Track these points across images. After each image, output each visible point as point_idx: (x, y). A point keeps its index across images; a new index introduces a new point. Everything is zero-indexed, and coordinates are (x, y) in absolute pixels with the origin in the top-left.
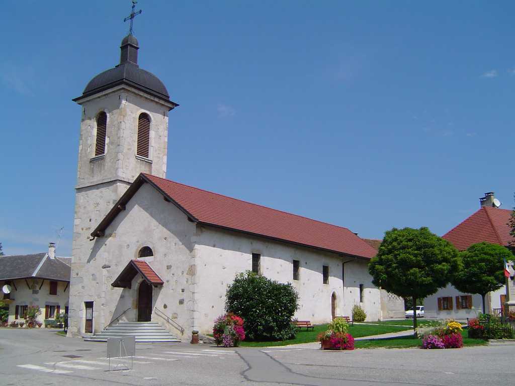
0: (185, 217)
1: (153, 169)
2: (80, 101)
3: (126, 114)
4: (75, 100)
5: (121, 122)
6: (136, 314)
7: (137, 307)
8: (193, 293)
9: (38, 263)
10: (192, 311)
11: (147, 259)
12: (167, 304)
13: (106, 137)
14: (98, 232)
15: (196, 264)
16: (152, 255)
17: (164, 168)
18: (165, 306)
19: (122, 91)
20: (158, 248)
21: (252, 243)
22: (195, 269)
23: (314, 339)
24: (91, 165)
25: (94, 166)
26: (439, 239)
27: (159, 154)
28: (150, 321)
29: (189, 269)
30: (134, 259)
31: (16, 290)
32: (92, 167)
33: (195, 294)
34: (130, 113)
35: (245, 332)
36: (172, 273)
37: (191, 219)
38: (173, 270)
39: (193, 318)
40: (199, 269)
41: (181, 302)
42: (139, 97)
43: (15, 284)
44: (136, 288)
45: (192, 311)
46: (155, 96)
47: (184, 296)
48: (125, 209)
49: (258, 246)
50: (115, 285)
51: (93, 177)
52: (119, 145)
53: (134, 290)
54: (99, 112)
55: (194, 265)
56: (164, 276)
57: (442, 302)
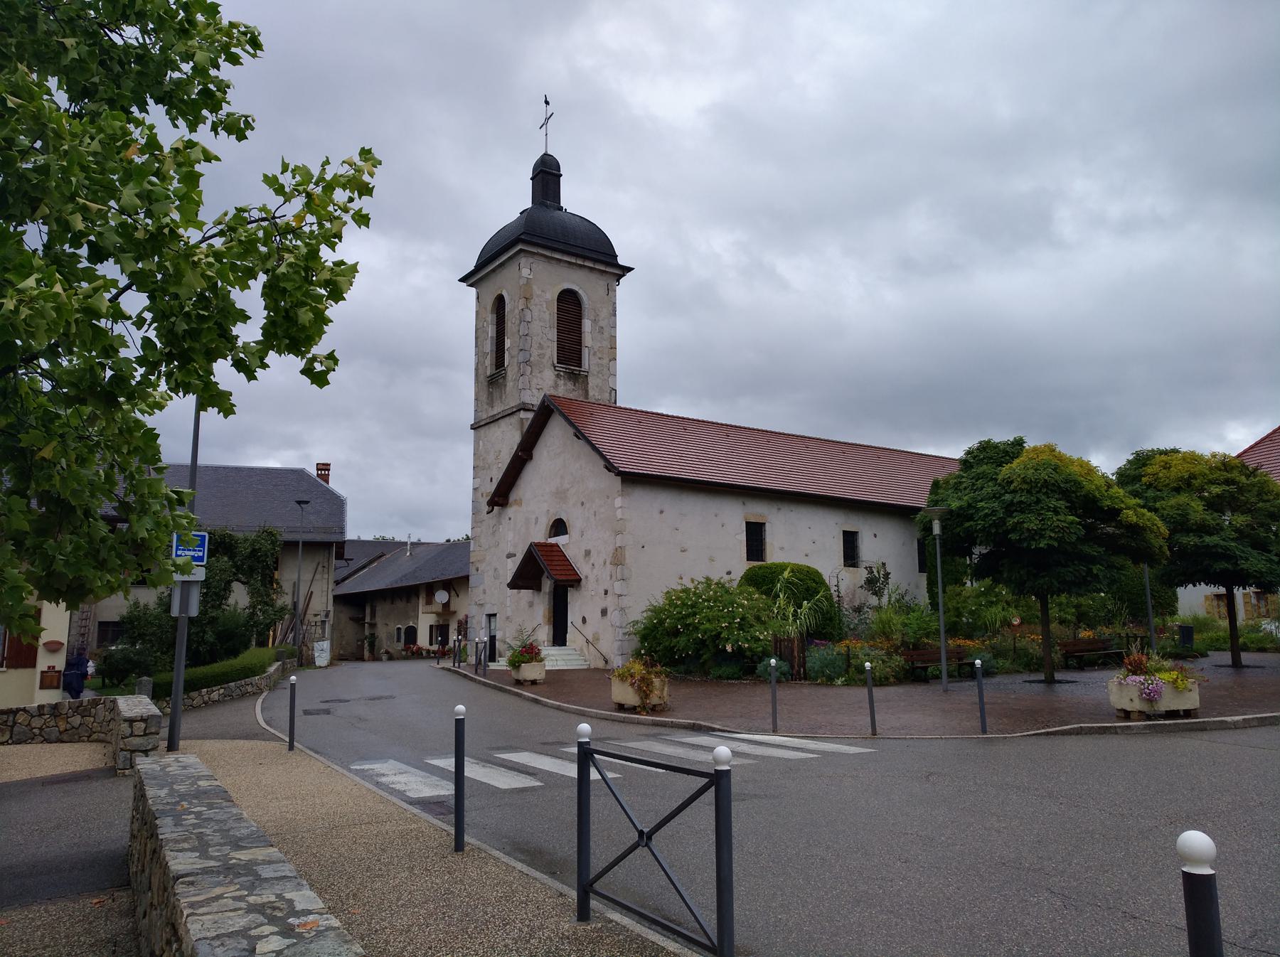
0: (602, 463)
1: (590, 384)
2: (471, 281)
3: (532, 295)
4: (462, 280)
6: (548, 634)
7: (548, 621)
11: (561, 540)
14: (496, 499)
16: (566, 533)
18: (584, 620)
19: (522, 255)
20: (575, 521)
21: (744, 504)
23: (1221, 714)
24: (489, 388)
25: (492, 388)
27: (600, 358)
28: (565, 645)
29: (614, 554)
31: (458, 596)
32: (491, 390)
34: (539, 292)
36: (592, 561)
37: (610, 467)
41: (604, 612)
42: (554, 262)
43: (456, 589)
44: (548, 591)
46: (585, 258)
47: (610, 602)
48: (531, 458)
49: (758, 511)
50: (514, 585)
51: (492, 407)
53: (545, 593)
56: (583, 568)
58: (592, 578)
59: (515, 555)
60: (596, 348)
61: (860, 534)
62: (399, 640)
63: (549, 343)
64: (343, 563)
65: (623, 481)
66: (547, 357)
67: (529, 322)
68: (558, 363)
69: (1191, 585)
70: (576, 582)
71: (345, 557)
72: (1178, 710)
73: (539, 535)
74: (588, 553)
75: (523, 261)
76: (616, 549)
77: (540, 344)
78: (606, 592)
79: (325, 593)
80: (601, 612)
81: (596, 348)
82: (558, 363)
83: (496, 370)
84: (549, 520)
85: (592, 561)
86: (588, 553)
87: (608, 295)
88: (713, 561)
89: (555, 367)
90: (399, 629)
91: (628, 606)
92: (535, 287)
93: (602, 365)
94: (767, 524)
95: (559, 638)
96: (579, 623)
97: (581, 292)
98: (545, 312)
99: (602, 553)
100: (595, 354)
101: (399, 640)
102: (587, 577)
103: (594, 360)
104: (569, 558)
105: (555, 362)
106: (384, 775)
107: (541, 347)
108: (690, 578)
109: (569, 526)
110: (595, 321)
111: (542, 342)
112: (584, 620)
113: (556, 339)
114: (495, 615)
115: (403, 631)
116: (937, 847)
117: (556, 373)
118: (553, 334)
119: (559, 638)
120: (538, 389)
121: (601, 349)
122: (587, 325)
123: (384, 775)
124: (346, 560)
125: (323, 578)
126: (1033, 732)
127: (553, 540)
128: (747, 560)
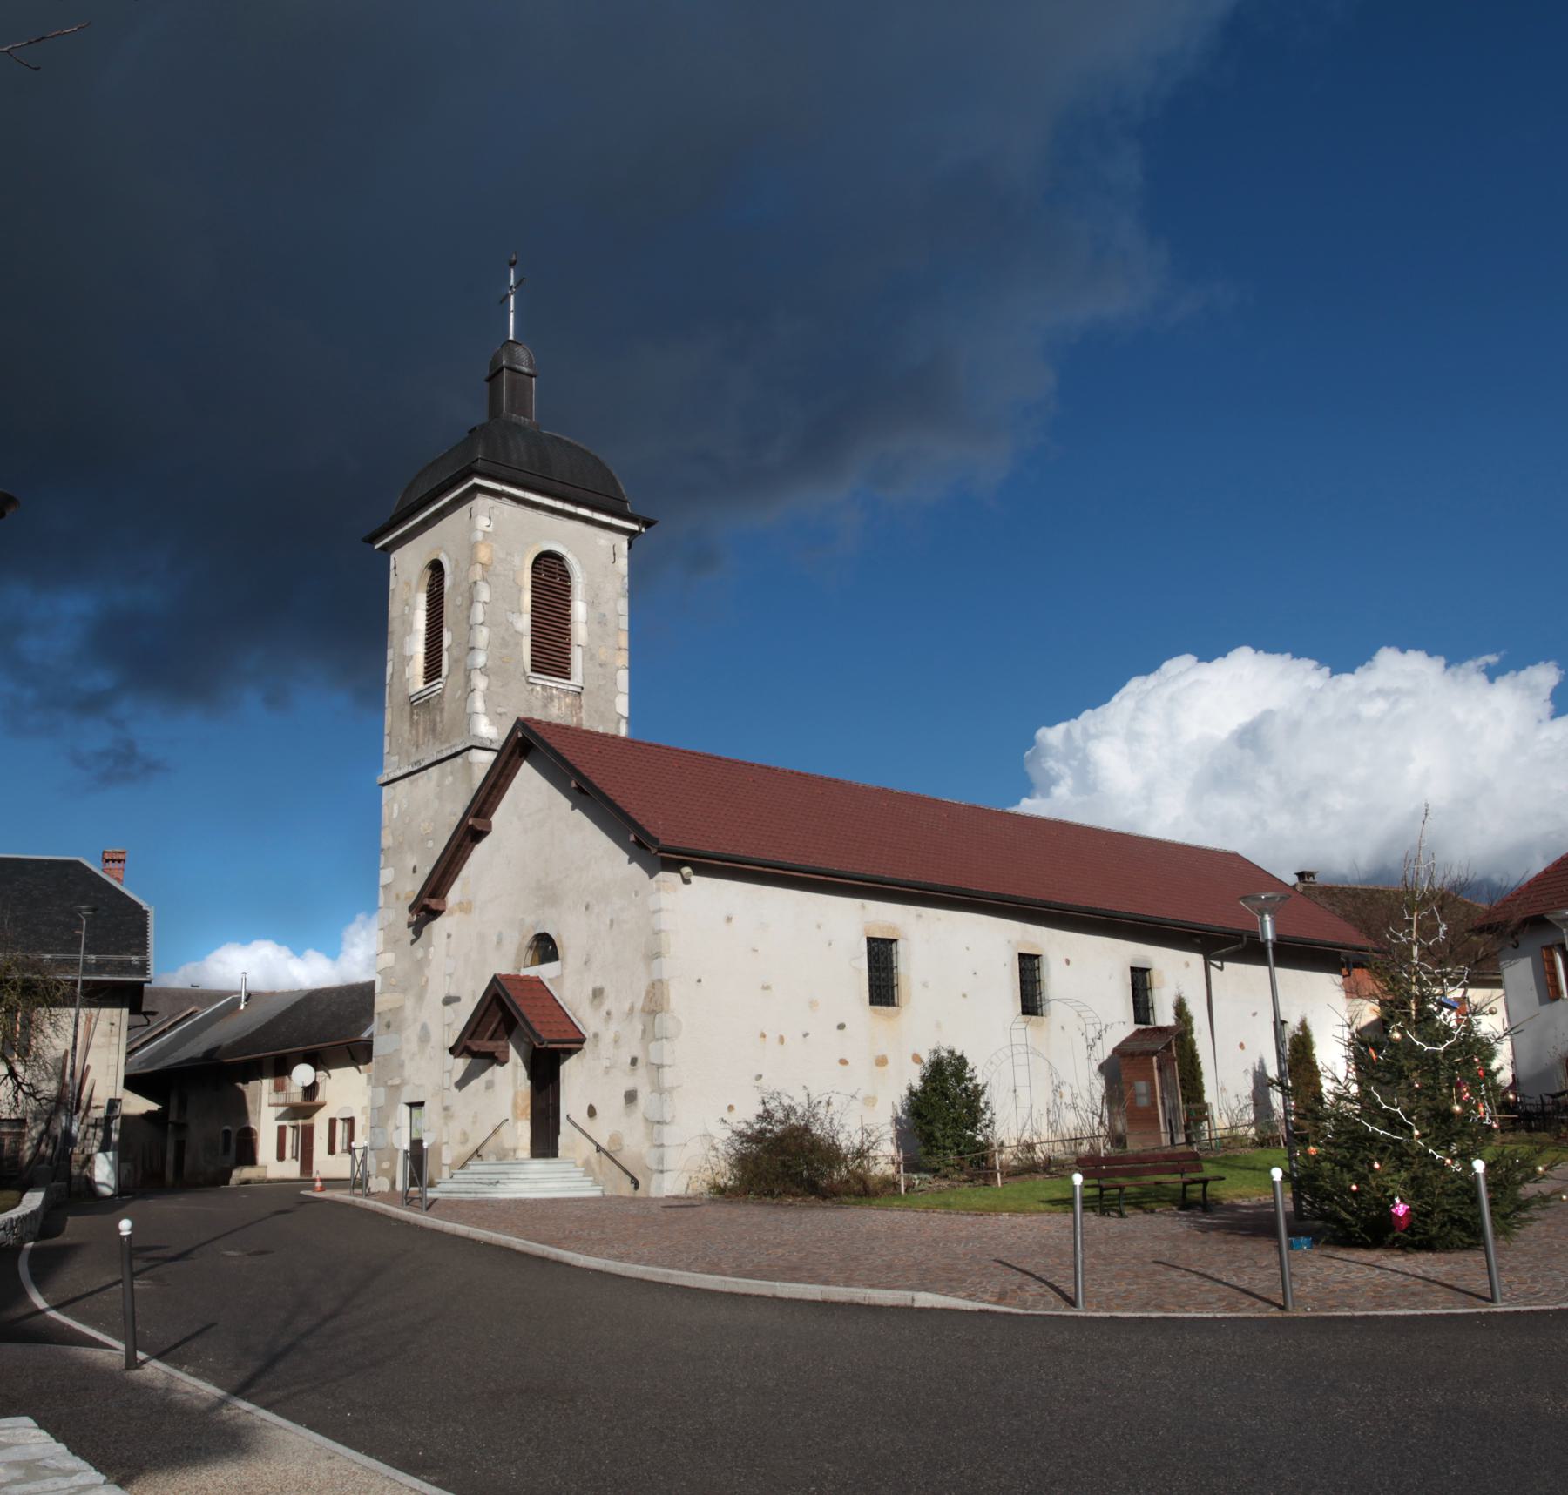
5: (475, 583)
8: (660, 1067)
9: (222, 1000)
10: (658, 1122)
11: (546, 972)
12: (595, 1105)
13: (445, 630)
15: (665, 976)
17: (622, 705)
18: (592, 1112)
22: (662, 993)
26: (498, 728)
28: (555, 1155)
30: (505, 969)
33: (666, 1070)
35: (916, 1177)
38: (609, 1003)
39: (662, 1146)
40: (677, 997)
41: (631, 1097)
45: (658, 1122)
52: (472, 649)
54: (428, 561)
55: (660, 980)
56: (587, 1019)
57: (1172, 1179)
58: (607, 1036)
59: (457, 999)
61: (1043, 961)
62: (227, 1149)
64: (141, 1019)
68: (532, 671)
70: (574, 1042)
71: (144, 1009)
72: (143, 947)
73: (507, 960)
74: (598, 993)
75: (482, 502)
76: (653, 984)
77: (503, 638)
78: (634, 1061)
79: (113, 1070)
80: (625, 1096)
82: (532, 671)
83: (426, 683)
84: (523, 937)
85: (605, 1008)
86: (598, 993)
87: (614, 562)
90: (227, 1133)
94: (900, 943)
95: (545, 1141)
96: (581, 1117)
99: (625, 995)
101: (227, 1149)
102: (596, 1035)
104: (561, 1003)
105: (528, 668)
108: (777, 1036)
109: (562, 946)
112: (592, 1112)
113: (572, 648)
114: (421, 1104)
115: (233, 1136)
116: (1400, 1465)
117: (530, 687)
119: (545, 1141)
120: (500, 714)
124: (146, 1014)
125: (110, 1044)
127: (531, 972)
128: (872, 1003)
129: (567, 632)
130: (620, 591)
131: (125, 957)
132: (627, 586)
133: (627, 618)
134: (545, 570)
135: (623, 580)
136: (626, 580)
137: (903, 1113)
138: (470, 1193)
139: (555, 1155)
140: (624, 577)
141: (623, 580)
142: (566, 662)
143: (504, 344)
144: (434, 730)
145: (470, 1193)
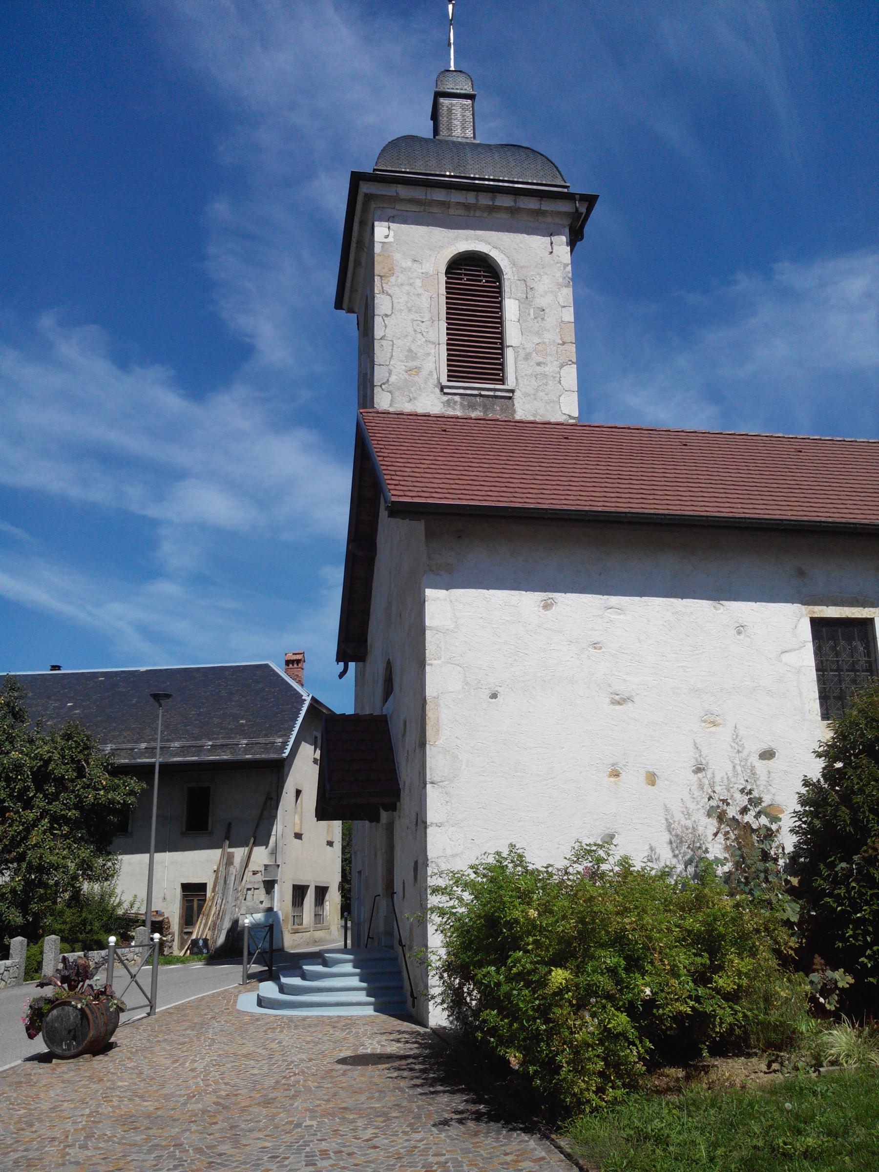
27: (539, 364)
60: (529, 346)
63: (431, 349)
65: (430, 535)
66: (424, 373)
67: (387, 316)
69: (637, 866)
77: (410, 351)
81: (529, 346)
82: (449, 381)
87: (552, 252)
88: (714, 724)
89: (442, 388)
91: (449, 852)
92: (397, 256)
93: (545, 376)
97: (494, 254)
98: (419, 295)
100: (527, 357)
103: (526, 368)
106: (421, 1094)
107: (411, 355)
110: (526, 301)
111: (413, 348)
117: (446, 398)
118: (439, 331)
121: (540, 348)
122: (511, 308)
123: (421, 1094)
126: (516, 186)
129: (501, 336)
130: (561, 280)
131: (271, 739)
132: (570, 275)
133: (572, 310)
134: (466, 275)
135: (565, 268)
136: (569, 268)
137: (823, 1044)
138: (411, 201)
139: (318, 820)
140: (566, 265)
141: (565, 268)
142: (502, 367)
143: (442, 72)
144: (298, 661)
145: (411, 201)
